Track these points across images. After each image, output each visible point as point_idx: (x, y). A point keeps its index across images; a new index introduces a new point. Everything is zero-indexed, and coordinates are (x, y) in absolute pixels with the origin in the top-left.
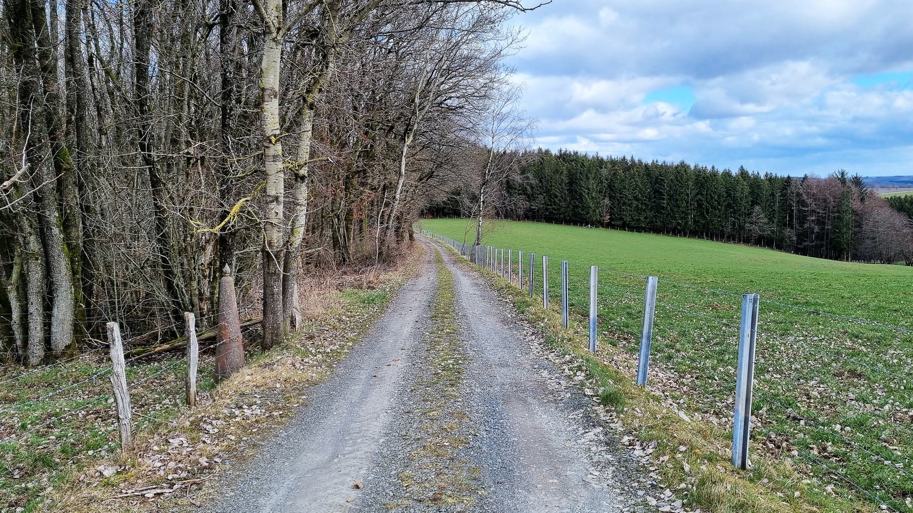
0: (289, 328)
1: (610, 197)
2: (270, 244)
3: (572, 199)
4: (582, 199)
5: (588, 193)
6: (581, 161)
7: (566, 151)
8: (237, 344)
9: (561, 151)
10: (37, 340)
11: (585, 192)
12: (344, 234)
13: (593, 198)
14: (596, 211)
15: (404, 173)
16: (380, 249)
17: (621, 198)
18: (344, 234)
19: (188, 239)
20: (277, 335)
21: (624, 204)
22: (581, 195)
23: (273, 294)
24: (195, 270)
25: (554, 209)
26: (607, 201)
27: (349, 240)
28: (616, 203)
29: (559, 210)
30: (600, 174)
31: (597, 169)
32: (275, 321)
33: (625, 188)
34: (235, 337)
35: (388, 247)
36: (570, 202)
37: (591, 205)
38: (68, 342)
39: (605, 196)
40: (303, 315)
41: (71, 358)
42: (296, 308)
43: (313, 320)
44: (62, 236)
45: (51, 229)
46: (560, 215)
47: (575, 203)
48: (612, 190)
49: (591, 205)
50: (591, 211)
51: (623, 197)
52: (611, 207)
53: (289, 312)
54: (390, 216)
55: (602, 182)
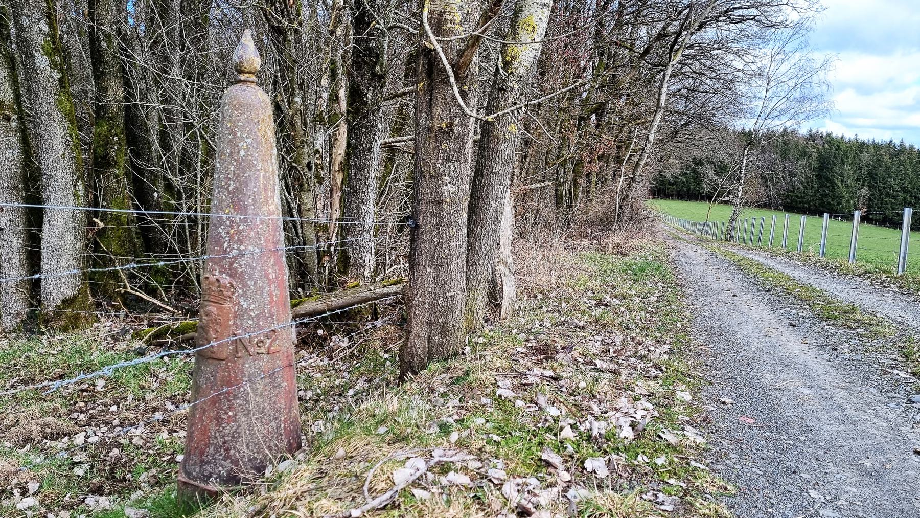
0: (481, 310)
1: (870, 187)
2: (439, 25)
3: (821, 187)
4: (833, 187)
5: (842, 181)
6: (836, 143)
7: (817, 132)
8: (264, 363)
9: (811, 131)
10: (12, 282)
11: (837, 179)
12: (570, 189)
13: (847, 186)
14: (849, 202)
15: (663, 104)
16: (620, 207)
17: (884, 188)
18: (570, 189)
19: (296, 99)
20: (445, 331)
21: (888, 195)
22: (832, 182)
23: (439, 203)
24: (310, 169)
25: (797, 197)
26: (865, 191)
27: (576, 198)
28: (877, 193)
29: (802, 198)
30: (860, 160)
31: (856, 154)
32: (442, 291)
33: (890, 177)
34: (257, 336)
35: (632, 206)
36: (818, 190)
37: (844, 194)
38: (70, 293)
39: (863, 185)
40: (519, 283)
41: (74, 323)
42: (506, 264)
43: (540, 296)
44: (56, 75)
45: (33, 56)
46: (804, 203)
47: (824, 191)
48: (874, 178)
49: (844, 194)
50: (844, 201)
51: (887, 188)
52: (870, 199)
53: (484, 268)
54: (638, 163)
55: (860, 169)
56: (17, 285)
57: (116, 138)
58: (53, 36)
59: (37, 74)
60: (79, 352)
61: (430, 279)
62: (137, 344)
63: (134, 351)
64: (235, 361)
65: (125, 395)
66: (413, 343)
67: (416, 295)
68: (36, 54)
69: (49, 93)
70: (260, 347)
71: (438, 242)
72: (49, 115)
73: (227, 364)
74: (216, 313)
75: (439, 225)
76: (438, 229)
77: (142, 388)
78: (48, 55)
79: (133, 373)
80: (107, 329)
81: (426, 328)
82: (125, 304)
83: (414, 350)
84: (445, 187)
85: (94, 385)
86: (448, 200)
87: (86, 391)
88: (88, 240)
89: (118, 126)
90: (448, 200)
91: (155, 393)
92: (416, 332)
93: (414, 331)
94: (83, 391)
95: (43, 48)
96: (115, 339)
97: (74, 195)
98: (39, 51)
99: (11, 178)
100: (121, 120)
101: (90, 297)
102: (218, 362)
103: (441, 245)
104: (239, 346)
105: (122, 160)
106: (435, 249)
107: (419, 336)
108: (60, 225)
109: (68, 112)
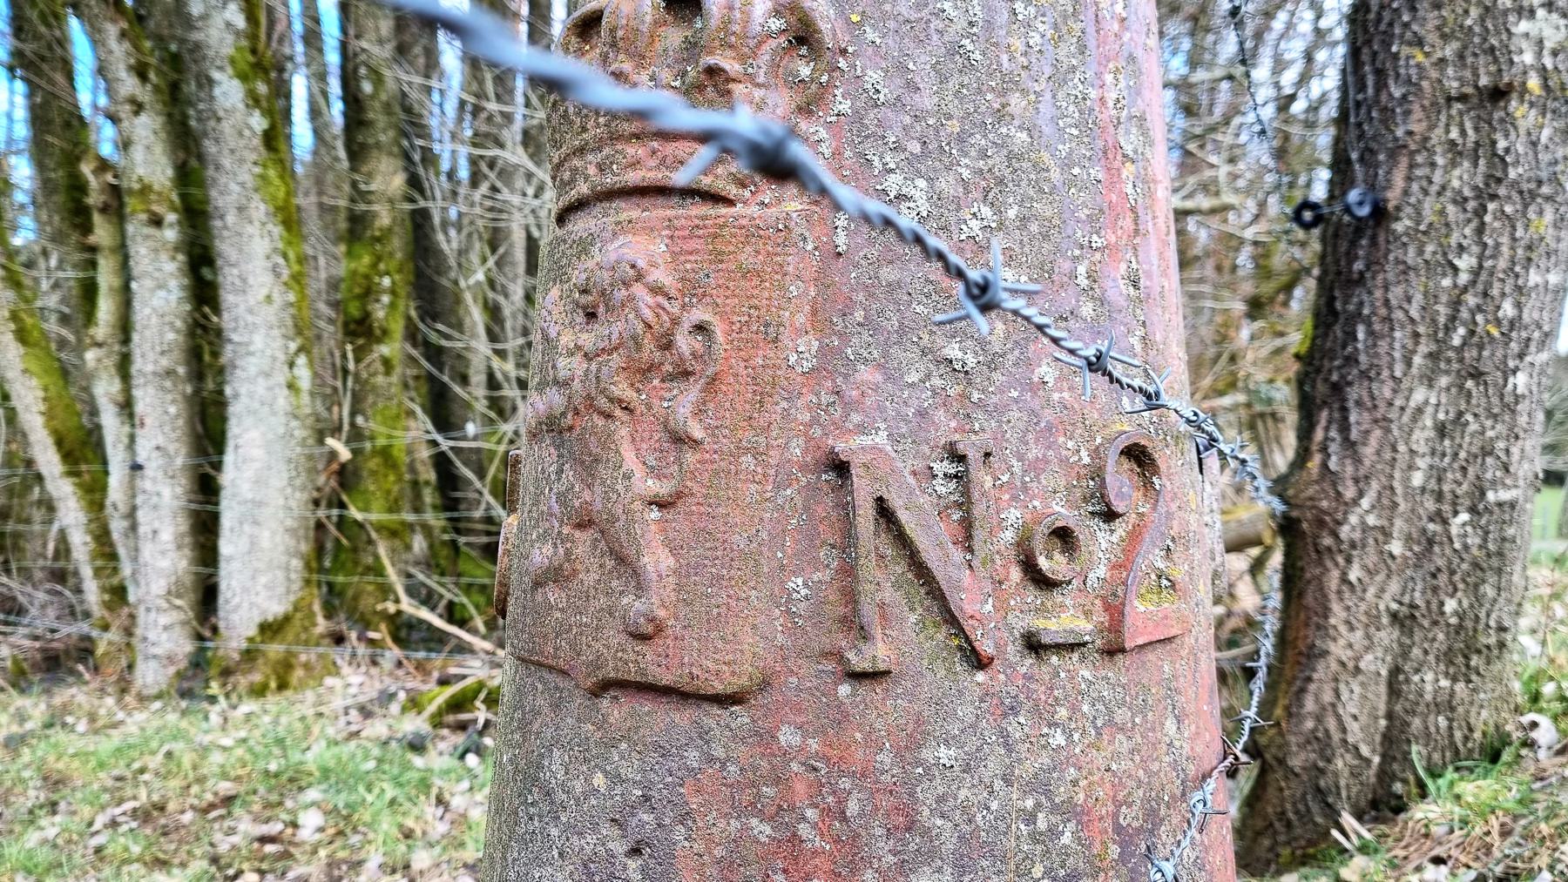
44: (258, 122)
45: (211, 82)
56: (169, 593)
57: (386, 281)
58: (253, 37)
59: (219, 120)
60: (280, 742)
61: (1422, 436)
62: (414, 724)
63: (399, 741)
64: (841, 717)
65: (362, 855)
66: (1328, 697)
67: (1355, 502)
68: (216, 75)
69: (242, 161)
70: (1043, 582)
71: (1476, 272)
72: (241, 209)
73: (765, 738)
74: (661, 276)
75: (1485, 195)
76: (1481, 211)
77: (408, 835)
78: (243, 77)
79: (389, 794)
80: (353, 690)
81: (1388, 636)
82: (398, 640)
83: (1331, 724)
84: (1524, 26)
85: (295, 825)
86: (1534, 83)
87: (271, 840)
88: (318, 489)
89: (391, 255)
90: (1534, 83)
91: (438, 849)
92: (1346, 655)
93: (1338, 649)
94: (264, 840)
95: (232, 61)
96: (366, 713)
97: (291, 386)
98: (221, 68)
99: (163, 353)
100: (397, 246)
101: (320, 620)
102: (682, 717)
103: (1489, 284)
104: (869, 569)
105: (397, 327)
106: (1456, 304)
107: (1357, 670)
108: (257, 453)
109: (280, 203)
